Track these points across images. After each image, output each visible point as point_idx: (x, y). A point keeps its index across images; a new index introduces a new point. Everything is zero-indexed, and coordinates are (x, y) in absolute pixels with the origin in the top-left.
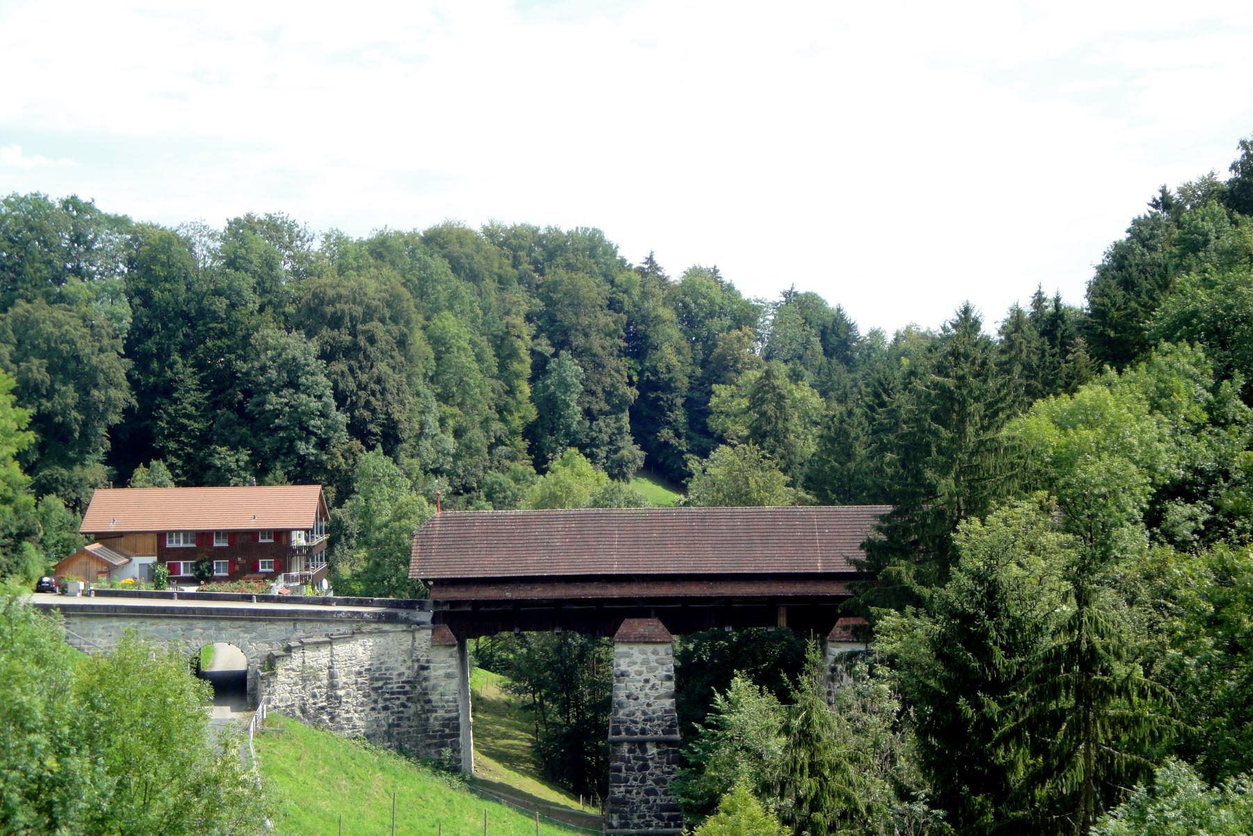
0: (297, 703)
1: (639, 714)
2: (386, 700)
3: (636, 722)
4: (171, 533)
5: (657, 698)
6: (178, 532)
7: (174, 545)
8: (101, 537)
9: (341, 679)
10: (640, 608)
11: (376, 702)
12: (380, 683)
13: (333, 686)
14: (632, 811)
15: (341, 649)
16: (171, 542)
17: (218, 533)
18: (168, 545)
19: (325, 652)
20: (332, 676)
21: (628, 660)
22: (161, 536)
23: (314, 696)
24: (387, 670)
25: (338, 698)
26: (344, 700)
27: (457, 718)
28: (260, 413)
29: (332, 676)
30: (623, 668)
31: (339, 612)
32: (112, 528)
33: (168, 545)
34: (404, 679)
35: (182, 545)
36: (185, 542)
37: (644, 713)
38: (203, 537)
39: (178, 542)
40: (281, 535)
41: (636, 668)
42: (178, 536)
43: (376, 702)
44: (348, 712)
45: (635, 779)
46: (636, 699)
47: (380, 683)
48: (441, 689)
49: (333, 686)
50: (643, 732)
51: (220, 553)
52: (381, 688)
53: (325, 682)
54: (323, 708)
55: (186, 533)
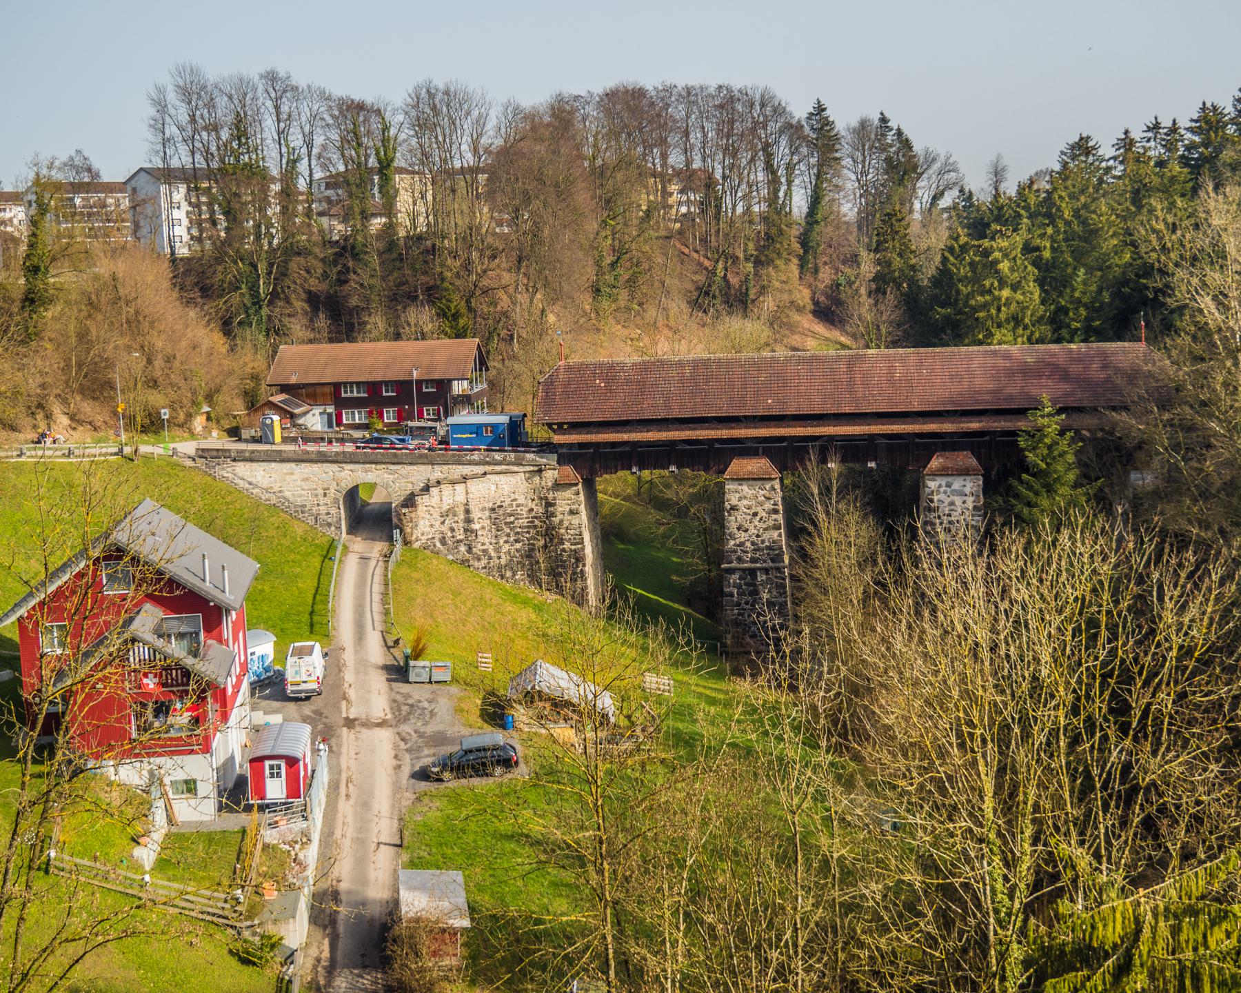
0: (438, 536)
1: (748, 544)
2: (518, 533)
3: (746, 552)
4: (345, 384)
5: (765, 529)
6: (351, 384)
7: (349, 395)
8: (285, 388)
9: (476, 514)
10: (747, 449)
11: (508, 535)
12: (512, 519)
13: (468, 521)
14: (745, 632)
15: (475, 487)
16: (346, 392)
17: (387, 383)
18: (343, 395)
19: (460, 488)
20: (467, 512)
21: (737, 495)
22: (337, 386)
23: (452, 530)
24: (518, 506)
25: (472, 531)
26: (480, 533)
27: (583, 549)
28: (1218, 122)
29: (467, 512)
30: (734, 502)
31: (258, 451)
32: (293, 380)
33: (343, 395)
34: (533, 514)
35: (355, 394)
36: (358, 392)
37: (753, 543)
38: (373, 387)
39: (352, 392)
40: (443, 385)
41: (745, 502)
42: (351, 387)
43: (508, 535)
44: (483, 544)
45: (747, 603)
46: (746, 531)
47: (512, 519)
48: (566, 524)
49: (468, 521)
50: (754, 560)
51: (389, 402)
52: (512, 523)
53: (462, 517)
54: (461, 541)
55: (358, 384)
